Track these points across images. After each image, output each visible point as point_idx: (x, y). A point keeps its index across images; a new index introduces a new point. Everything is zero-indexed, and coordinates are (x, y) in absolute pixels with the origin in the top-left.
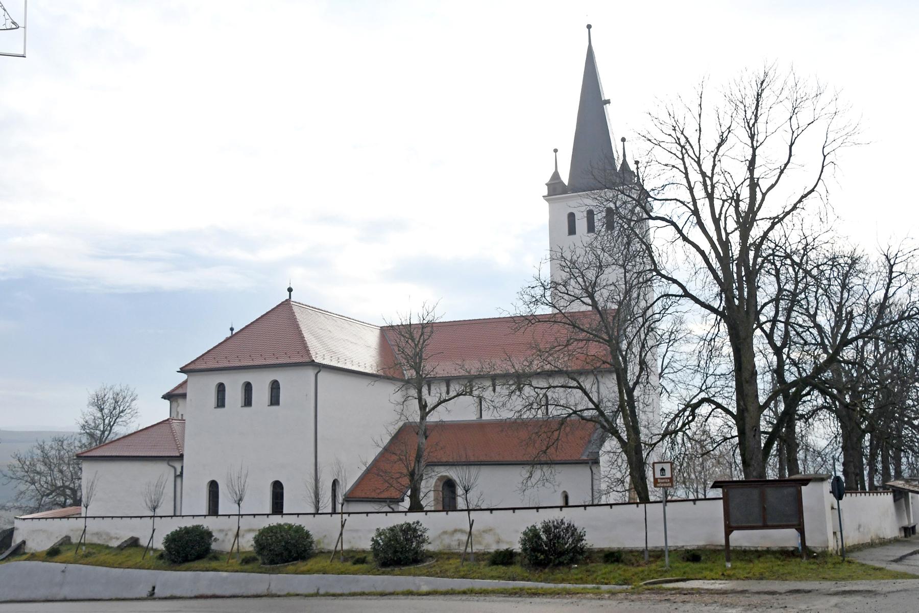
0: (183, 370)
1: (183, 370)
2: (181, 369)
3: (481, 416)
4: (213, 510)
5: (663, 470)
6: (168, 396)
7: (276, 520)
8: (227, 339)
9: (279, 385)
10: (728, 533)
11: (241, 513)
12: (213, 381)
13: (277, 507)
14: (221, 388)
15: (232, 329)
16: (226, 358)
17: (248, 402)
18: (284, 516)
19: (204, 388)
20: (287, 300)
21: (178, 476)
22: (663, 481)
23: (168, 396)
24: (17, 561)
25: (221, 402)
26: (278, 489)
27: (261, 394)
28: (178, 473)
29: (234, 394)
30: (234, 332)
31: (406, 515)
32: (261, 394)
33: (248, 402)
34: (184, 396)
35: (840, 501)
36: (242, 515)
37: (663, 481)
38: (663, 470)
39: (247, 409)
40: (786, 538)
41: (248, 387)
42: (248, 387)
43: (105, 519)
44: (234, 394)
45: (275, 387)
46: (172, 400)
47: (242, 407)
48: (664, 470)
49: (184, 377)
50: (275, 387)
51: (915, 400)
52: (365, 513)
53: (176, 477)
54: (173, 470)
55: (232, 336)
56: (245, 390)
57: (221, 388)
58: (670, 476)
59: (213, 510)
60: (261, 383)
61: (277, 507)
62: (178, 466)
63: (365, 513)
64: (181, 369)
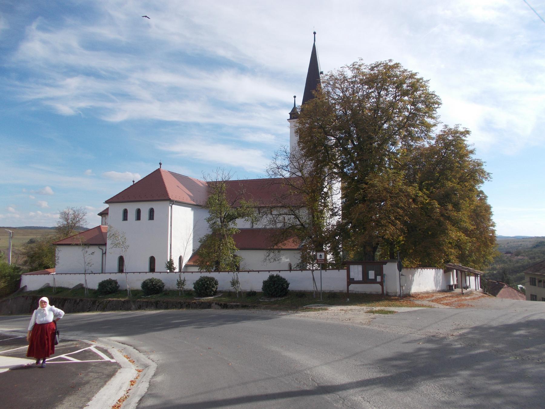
0: (107, 202)
1: (107, 202)
2: (105, 201)
3: (253, 227)
4: (121, 270)
5: (321, 255)
6: (101, 214)
7: (151, 276)
8: (131, 186)
9: (154, 210)
10: (348, 285)
11: (127, 272)
12: (122, 207)
13: (152, 269)
14: (125, 212)
15: (133, 182)
16: (123, 197)
17: (138, 218)
18: (240, 272)
19: (117, 210)
20: (159, 169)
21: (104, 253)
22: (321, 260)
23: (101, 214)
24: (252, 321)
25: (125, 218)
26: (152, 260)
27: (145, 215)
28: (104, 252)
29: (132, 215)
30: (135, 183)
31: (259, 273)
32: (145, 215)
33: (138, 218)
34: (107, 214)
35: (400, 272)
36: (128, 273)
37: (321, 260)
38: (321, 255)
39: (138, 221)
40: (375, 288)
41: (139, 212)
42: (139, 212)
43: (135, 273)
44: (132, 215)
45: (152, 211)
46: (102, 216)
47: (136, 220)
48: (321, 256)
49: (107, 206)
50: (152, 211)
51: (397, 229)
52: (268, 271)
53: (103, 254)
54: (101, 251)
55: (134, 184)
56: (137, 212)
57: (125, 212)
58: (324, 258)
59: (121, 270)
60: (145, 208)
61: (152, 269)
62: (104, 248)
63: (268, 271)
64: (105, 201)
